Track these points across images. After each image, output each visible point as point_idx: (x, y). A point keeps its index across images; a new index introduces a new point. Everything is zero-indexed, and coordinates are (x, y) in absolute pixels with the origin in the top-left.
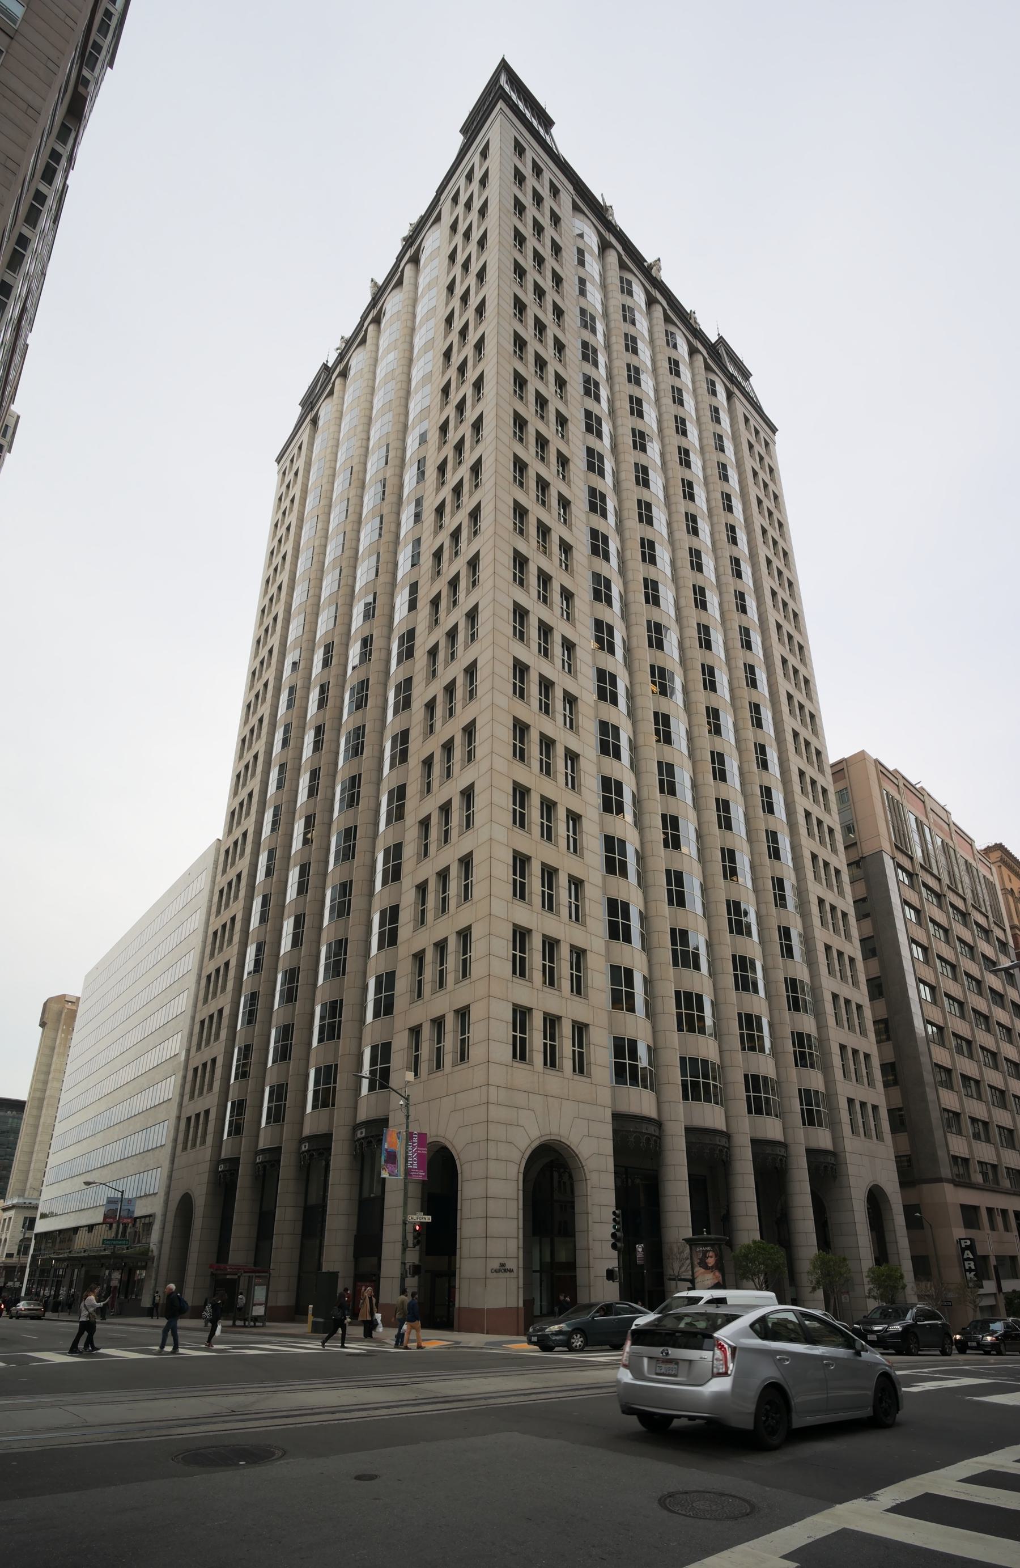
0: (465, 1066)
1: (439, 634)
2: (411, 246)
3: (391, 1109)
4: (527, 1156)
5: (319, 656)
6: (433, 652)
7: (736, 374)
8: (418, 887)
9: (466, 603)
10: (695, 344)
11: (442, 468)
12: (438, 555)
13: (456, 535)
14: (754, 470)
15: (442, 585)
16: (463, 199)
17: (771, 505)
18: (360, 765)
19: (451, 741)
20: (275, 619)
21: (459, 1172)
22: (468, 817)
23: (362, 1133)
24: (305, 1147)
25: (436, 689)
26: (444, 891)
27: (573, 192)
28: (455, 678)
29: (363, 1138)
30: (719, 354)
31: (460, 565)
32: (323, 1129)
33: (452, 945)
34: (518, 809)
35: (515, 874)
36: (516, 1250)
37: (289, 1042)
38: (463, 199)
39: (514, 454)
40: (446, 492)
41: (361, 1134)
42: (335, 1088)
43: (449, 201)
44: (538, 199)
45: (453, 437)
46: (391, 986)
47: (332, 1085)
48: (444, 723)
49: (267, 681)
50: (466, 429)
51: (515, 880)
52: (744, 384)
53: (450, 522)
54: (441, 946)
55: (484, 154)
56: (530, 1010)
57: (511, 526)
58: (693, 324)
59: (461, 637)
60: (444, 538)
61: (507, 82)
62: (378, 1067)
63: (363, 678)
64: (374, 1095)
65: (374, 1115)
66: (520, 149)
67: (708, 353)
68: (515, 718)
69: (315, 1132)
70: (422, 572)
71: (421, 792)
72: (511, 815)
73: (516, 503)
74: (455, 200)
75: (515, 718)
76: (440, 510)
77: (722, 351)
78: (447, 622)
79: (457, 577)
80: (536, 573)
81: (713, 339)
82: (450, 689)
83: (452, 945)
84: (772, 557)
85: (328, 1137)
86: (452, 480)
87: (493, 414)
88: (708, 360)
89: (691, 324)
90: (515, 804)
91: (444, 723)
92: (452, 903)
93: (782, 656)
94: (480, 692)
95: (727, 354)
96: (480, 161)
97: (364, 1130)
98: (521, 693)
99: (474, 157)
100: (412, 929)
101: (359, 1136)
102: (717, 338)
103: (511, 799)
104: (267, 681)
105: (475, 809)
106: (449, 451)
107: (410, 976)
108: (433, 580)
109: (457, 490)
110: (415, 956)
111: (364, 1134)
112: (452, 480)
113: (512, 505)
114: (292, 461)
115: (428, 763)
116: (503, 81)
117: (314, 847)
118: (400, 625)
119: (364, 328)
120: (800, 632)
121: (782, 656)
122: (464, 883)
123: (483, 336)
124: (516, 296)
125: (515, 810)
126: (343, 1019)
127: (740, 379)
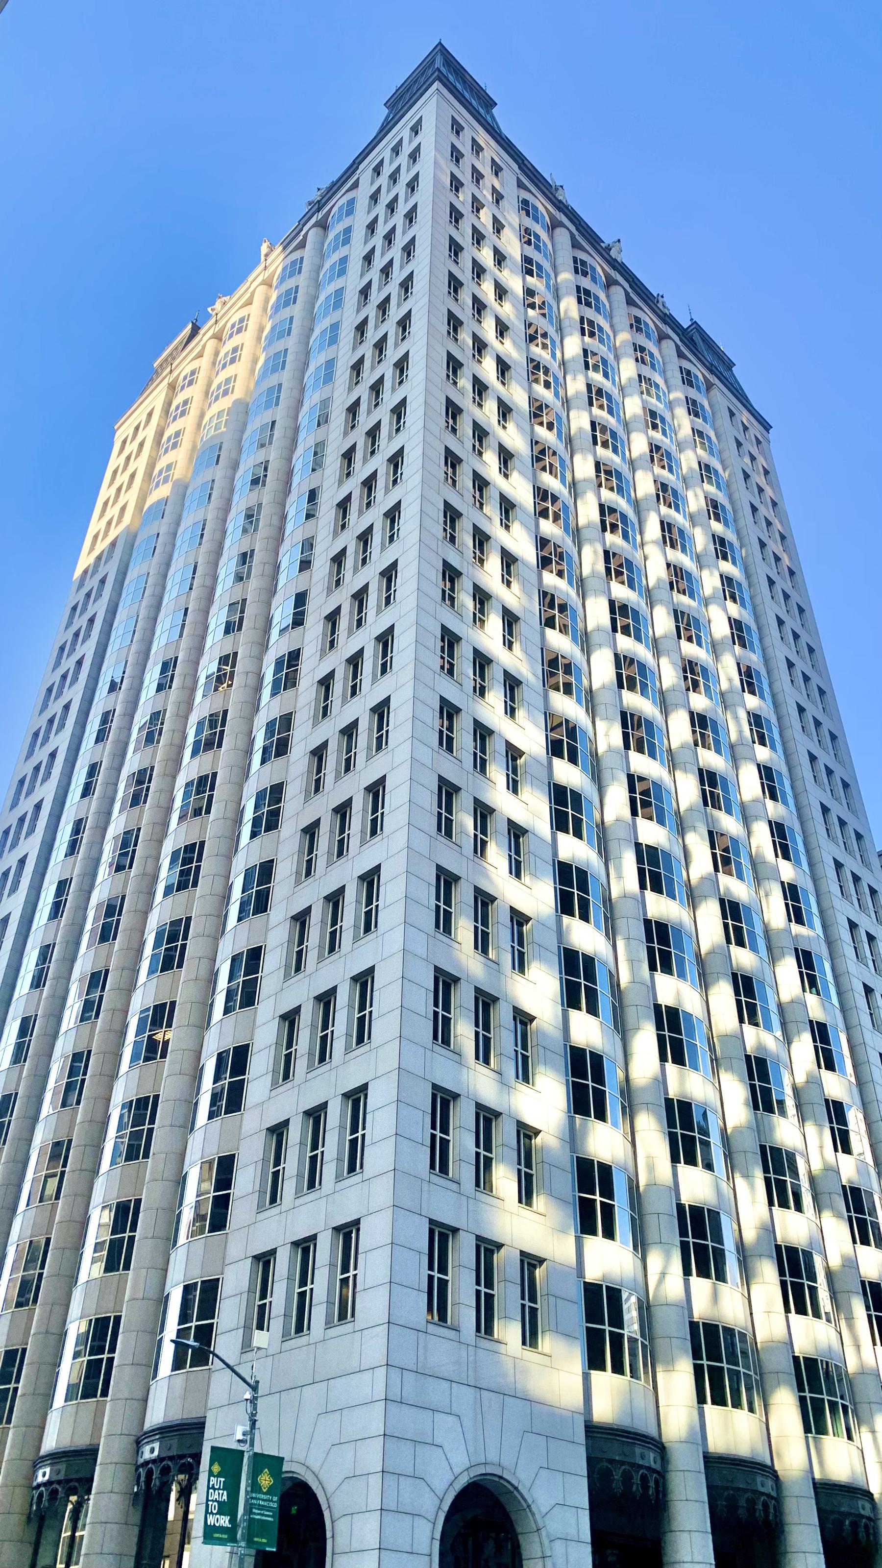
0: (347, 1328)
1: (336, 661)
2: (318, 210)
3: (210, 1404)
4: (446, 1507)
5: (152, 675)
6: (333, 618)
7: (715, 363)
8: (284, 1017)
9: (376, 624)
10: (664, 329)
11: (348, 456)
12: (338, 559)
13: (365, 538)
14: (769, 579)
15: (343, 597)
16: (387, 170)
17: (787, 585)
18: (203, 829)
19: (348, 803)
20: (91, 621)
21: (329, 1534)
22: (368, 914)
23: (152, 1451)
24: (43, 1475)
25: (330, 730)
26: (325, 1027)
27: (518, 171)
28: (376, 470)
29: (154, 1461)
30: (693, 340)
31: (370, 575)
32: (82, 1441)
33: (335, 1116)
34: (442, 906)
35: (436, 1005)
36: (428, 1541)
37: (12, 1386)
38: (387, 170)
39: (446, 447)
40: (353, 485)
41: (151, 1451)
42: (111, 1361)
43: (370, 171)
44: (477, 176)
45: (365, 422)
46: (209, 1307)
47: (105, 1356)
48: (330, 863)
49: (70, 702)
50: (383, 413)
51: (436, 1014)
52: (725, 374)
53: (357, 523)
54: (326, 999)
55: (416, 130)
56: (455, 1231)
57: (441, 534)
58: (661, 307)
59: (368, 665)
60: (348, 540)
61: (444, 65)
62: (193, 1324)
63: (180, 914)
64: (200, 1242)
65: (177, 1415)
66: (457, 128)
67: (681, 340)
68: (441, 778)
69: (67, 1443)
70: (314, 579)
71: (287, 966)
72: (437, 735)
73: (447, 505)
74: (377, 171)
75: (441, 778)
76: (344, 505)
77: (697, 338)
78: (347, 647)
79: (365, 589)
80: (471, 656)
81: (685, 324)
82: (355, 661)
83: (335, 1116)
84: (794, 659)
85: (91, 1453)
86: (362, 472)
87: (419, 451)
88: (682, 348)
89: (658, 308)
90: (438, 898)
91: (337, 778)
92: (338, 1046)
93: (821, 803)
94: (389, 823)
95: (703, 341)
96: (410, 136)
97: (156, 1445)
98: (447, 743)
99: (402, 130)
100: (311, 726)
101: (147, 1455)
102: (690, 323)
103: (433, 890)
104: (70, 702)
105: (386, 810)
106: (359, 436)
107: (245, 1296)
108: (323, 654)
109: (369, 483)
110: (257, 1258)
111: (156, 1453)
112: (362, 472)
113: (442, 507)
114: (137, 428)
115: (301, 919)
116: (439, 63)
117: (132, 874)
118: (278, 646)
119: (250, 290)
120: (819, 673)
121: (821, 803)
122: (349, 1138)
123: (415, 206)
124: (450, 274)
125: (438, 907)
126: (137, 1234)
127: (721, 369)
